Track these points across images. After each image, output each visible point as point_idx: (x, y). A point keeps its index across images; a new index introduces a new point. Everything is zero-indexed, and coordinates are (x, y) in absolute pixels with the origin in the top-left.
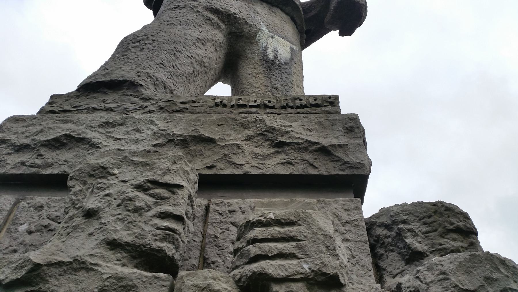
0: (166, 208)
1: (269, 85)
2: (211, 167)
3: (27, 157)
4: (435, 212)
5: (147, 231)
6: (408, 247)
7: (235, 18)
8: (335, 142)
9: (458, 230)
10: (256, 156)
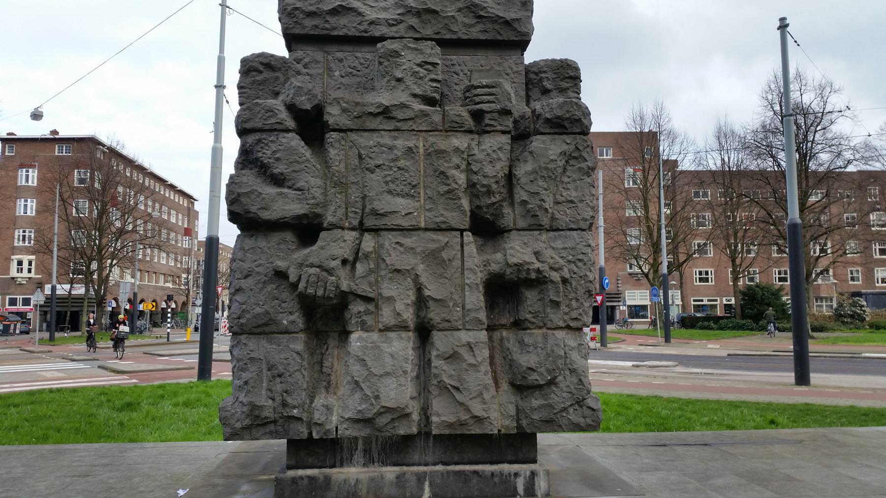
2: (438, 33)
3: (316, 21)
5: (427, 88)
6: (543, 86)
9: (571, 78)
10: (465, 25)
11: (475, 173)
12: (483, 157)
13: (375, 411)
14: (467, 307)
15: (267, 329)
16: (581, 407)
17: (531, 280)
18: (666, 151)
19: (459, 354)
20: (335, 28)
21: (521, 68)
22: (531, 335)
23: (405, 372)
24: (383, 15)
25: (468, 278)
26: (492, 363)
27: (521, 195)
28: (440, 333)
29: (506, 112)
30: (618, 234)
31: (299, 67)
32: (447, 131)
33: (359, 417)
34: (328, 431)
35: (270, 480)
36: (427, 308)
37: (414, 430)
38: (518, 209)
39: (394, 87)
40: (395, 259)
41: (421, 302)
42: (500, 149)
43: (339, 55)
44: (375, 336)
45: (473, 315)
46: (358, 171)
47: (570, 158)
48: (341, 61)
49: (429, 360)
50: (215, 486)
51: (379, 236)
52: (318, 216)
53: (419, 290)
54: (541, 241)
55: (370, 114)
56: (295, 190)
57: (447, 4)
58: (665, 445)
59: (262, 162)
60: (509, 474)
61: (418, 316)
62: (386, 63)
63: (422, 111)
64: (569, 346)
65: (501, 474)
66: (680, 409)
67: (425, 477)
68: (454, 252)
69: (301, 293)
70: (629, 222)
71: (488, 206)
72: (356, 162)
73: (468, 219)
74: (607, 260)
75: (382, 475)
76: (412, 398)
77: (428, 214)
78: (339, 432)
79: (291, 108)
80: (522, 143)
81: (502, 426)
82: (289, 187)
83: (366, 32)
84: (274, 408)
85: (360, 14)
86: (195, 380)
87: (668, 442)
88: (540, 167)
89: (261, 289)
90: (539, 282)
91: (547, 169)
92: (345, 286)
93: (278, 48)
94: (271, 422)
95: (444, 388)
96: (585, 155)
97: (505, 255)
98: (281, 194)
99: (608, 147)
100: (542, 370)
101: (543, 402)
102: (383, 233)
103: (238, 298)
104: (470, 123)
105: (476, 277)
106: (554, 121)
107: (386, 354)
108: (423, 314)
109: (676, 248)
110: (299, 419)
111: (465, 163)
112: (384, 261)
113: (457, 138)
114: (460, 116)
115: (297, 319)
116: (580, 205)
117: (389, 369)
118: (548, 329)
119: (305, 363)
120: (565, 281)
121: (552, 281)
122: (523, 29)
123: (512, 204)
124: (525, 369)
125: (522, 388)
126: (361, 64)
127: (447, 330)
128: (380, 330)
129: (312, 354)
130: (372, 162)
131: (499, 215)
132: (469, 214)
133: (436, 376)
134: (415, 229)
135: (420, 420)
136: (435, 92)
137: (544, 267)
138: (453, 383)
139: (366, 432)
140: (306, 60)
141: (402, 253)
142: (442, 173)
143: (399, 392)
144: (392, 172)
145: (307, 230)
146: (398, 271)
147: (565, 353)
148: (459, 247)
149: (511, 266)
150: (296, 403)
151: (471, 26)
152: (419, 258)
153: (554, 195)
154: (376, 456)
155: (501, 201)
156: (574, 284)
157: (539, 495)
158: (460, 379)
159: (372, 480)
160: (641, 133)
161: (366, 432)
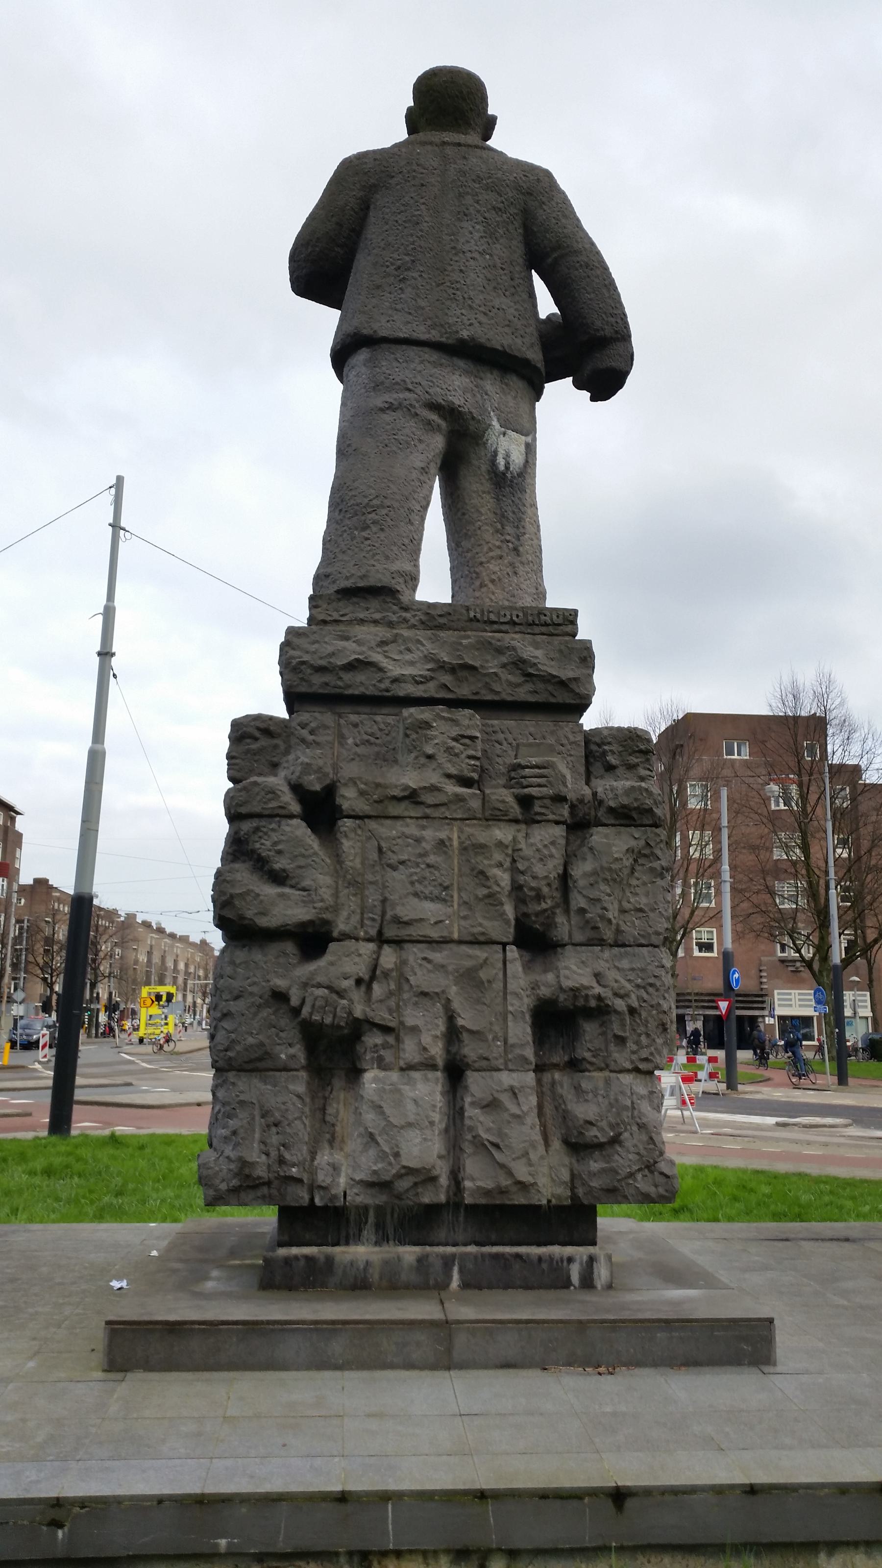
0: (471, 752)
1: (498, 512)
2: (477, 693)
3: (327, 678)
4: (630, 738)
6: (607, 762)
7: (460, 412)
8: (571, 674)
10: (510, 684)
11: (522, 873)
12: (532, 854)
13: (394, 1171)
14: (511, 1041)
15: (259, 1065)
16: (652, 1172)
17: (591, 1008)
18: (838, 751)
19: (500, 1101)
20: (349, 686)
21: (580, 738)
22: (590, 1078)
23: (432, 1123)
24: (408, 671)
25: (512, 1005)
26: (540, 1114)
27: (578, 901)
28: (476, 1074)
29: (560, 799)
30: (758, 892)
31: (305, 733)
32: (487, 820)
33: (374, 1179)
34: (335, 1197)
35: (253, 1266)
36: (460, 1041)
37: (442, 1198)
38: (575, 919)
39: (423, 765)
40: (421, 978)
41: (453, 1033)
42: (553, 843)
43: (354, 718)
44: (394, 1076)
45: (518, 1051)
46: (377, 868)
47: (640, 855)
48: (356, 725)
49: (462, 1109)
50: (175, 1271)
51: (402, 949)
52: (326, 923)
53: (451, 1018)
54: (603, 959)
55: (394, 798)
56: (299, 890)
57: (489, 657)
58: (787, 1240)
59: (259, 855)
60: (562, 1260)
61: (448, 1052)
62: (414, 736)
63: (456, 795)
64: (637, 1094)
65: (551, 1258)
66: (831, 1192)
67: (454, 1261)
68: (494, 971)
69: (304, 1020)
70: (778, 871)
71: (537, 914)
72: (375, 856)
73: (512, 930)
74: (738, 936)
75: (399, 1258)
76: (440, 1157)
77: (463, 923)
78: (349, 1198)
79: (297, 789)
80: (580, 833)
81: (553, 1195)
82: (292, 887)
83: (387, 691)
84: (269, 1165)
85: (381, 670)
86: (45, 1133)
87: (793, 1236)
88: (602, 868)
89: (255, 1014)
90: (600, 1011)
91: (610, 870)
92: (359, 1011)
93: (280, 711)
94: (264, 1184)
95: (480, 1145)
96: (658, 852)
97: (558, 977)
98: (281, 895)
99: (741, 740)
100: (604, 1124)
101: (605, 1165)
102: (406, 946)
103: (226, 1024)
104: (516, 810)
105: (521, 1004)
106: (620, 810)
107: (408, 1101)
108: (454, 1049)
109: (861, 915)
110: (300, 1181)
111: (509, 860)
112: (408, 980)
113: (500, 829)
114: (503, 802)
115: (298, 1051)
116: (651, 915)
117: (412, 1118)
118: (611, 1071)
119: (307, 1110)
120: (632, 1011)
121: (616, 1011)
122: (582, 691)
123: (567, 911)
124: (581, 1122)
125: (578, 1147)
126: (381, 730)
127: (485, 1070)
128: (402, 1069)
129: (313, 1098)
130: (395, 857)
131: (551, 924)
132: (513, 922)
133: (471, 1129)
134: (446, 941)
135: (449, 1186)
136: (474, 771)
137: (605, 993)
138: (492, 1139)
139: (381, 1199)
140: (313, 725)
141: (429, 971)
142: (482, 873)
143: (423, 1148)
144: (418, 870)
145: (313, 940)
146: (424, 994)
147: (633, 1103)
148: (500, 965)
149: (565, 991)
150: (295, 1159)
151: (518, 685)
152: (451, 977)
153: (620, 902)
154: (391, 1232)
155: (553, 907)
156: (644, 1014)
157: (599, 1287)
158: (500, 1134)
159: (386, 1263)
160: (796, 719)
161: (381, 1199)
